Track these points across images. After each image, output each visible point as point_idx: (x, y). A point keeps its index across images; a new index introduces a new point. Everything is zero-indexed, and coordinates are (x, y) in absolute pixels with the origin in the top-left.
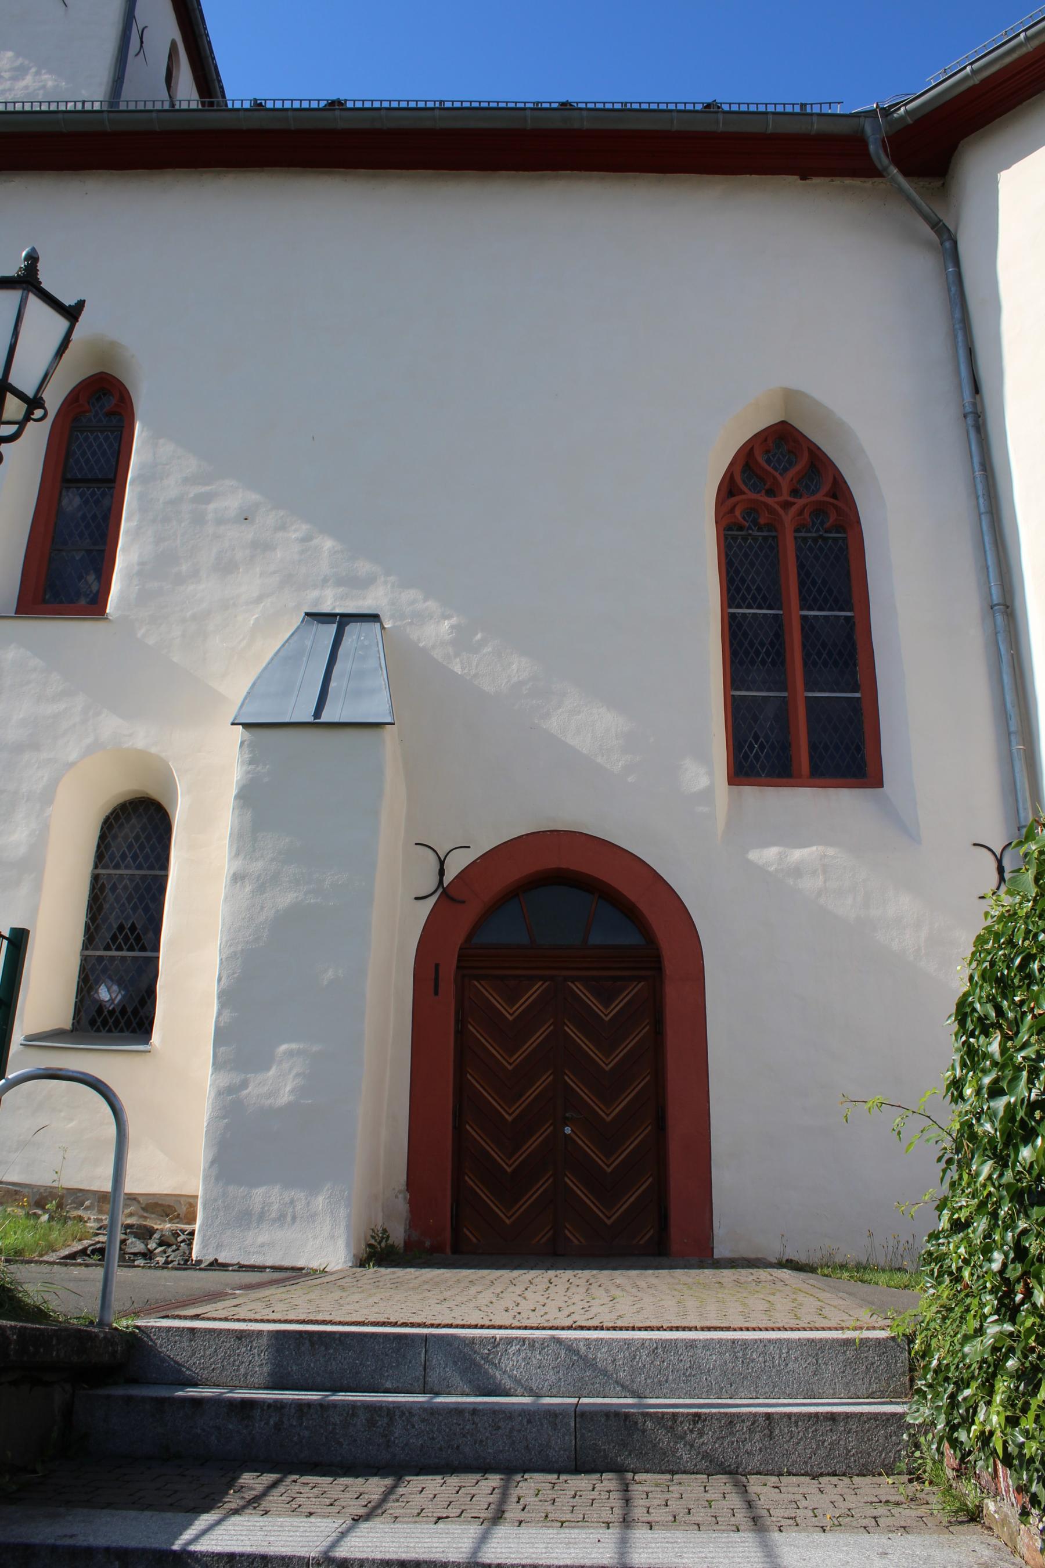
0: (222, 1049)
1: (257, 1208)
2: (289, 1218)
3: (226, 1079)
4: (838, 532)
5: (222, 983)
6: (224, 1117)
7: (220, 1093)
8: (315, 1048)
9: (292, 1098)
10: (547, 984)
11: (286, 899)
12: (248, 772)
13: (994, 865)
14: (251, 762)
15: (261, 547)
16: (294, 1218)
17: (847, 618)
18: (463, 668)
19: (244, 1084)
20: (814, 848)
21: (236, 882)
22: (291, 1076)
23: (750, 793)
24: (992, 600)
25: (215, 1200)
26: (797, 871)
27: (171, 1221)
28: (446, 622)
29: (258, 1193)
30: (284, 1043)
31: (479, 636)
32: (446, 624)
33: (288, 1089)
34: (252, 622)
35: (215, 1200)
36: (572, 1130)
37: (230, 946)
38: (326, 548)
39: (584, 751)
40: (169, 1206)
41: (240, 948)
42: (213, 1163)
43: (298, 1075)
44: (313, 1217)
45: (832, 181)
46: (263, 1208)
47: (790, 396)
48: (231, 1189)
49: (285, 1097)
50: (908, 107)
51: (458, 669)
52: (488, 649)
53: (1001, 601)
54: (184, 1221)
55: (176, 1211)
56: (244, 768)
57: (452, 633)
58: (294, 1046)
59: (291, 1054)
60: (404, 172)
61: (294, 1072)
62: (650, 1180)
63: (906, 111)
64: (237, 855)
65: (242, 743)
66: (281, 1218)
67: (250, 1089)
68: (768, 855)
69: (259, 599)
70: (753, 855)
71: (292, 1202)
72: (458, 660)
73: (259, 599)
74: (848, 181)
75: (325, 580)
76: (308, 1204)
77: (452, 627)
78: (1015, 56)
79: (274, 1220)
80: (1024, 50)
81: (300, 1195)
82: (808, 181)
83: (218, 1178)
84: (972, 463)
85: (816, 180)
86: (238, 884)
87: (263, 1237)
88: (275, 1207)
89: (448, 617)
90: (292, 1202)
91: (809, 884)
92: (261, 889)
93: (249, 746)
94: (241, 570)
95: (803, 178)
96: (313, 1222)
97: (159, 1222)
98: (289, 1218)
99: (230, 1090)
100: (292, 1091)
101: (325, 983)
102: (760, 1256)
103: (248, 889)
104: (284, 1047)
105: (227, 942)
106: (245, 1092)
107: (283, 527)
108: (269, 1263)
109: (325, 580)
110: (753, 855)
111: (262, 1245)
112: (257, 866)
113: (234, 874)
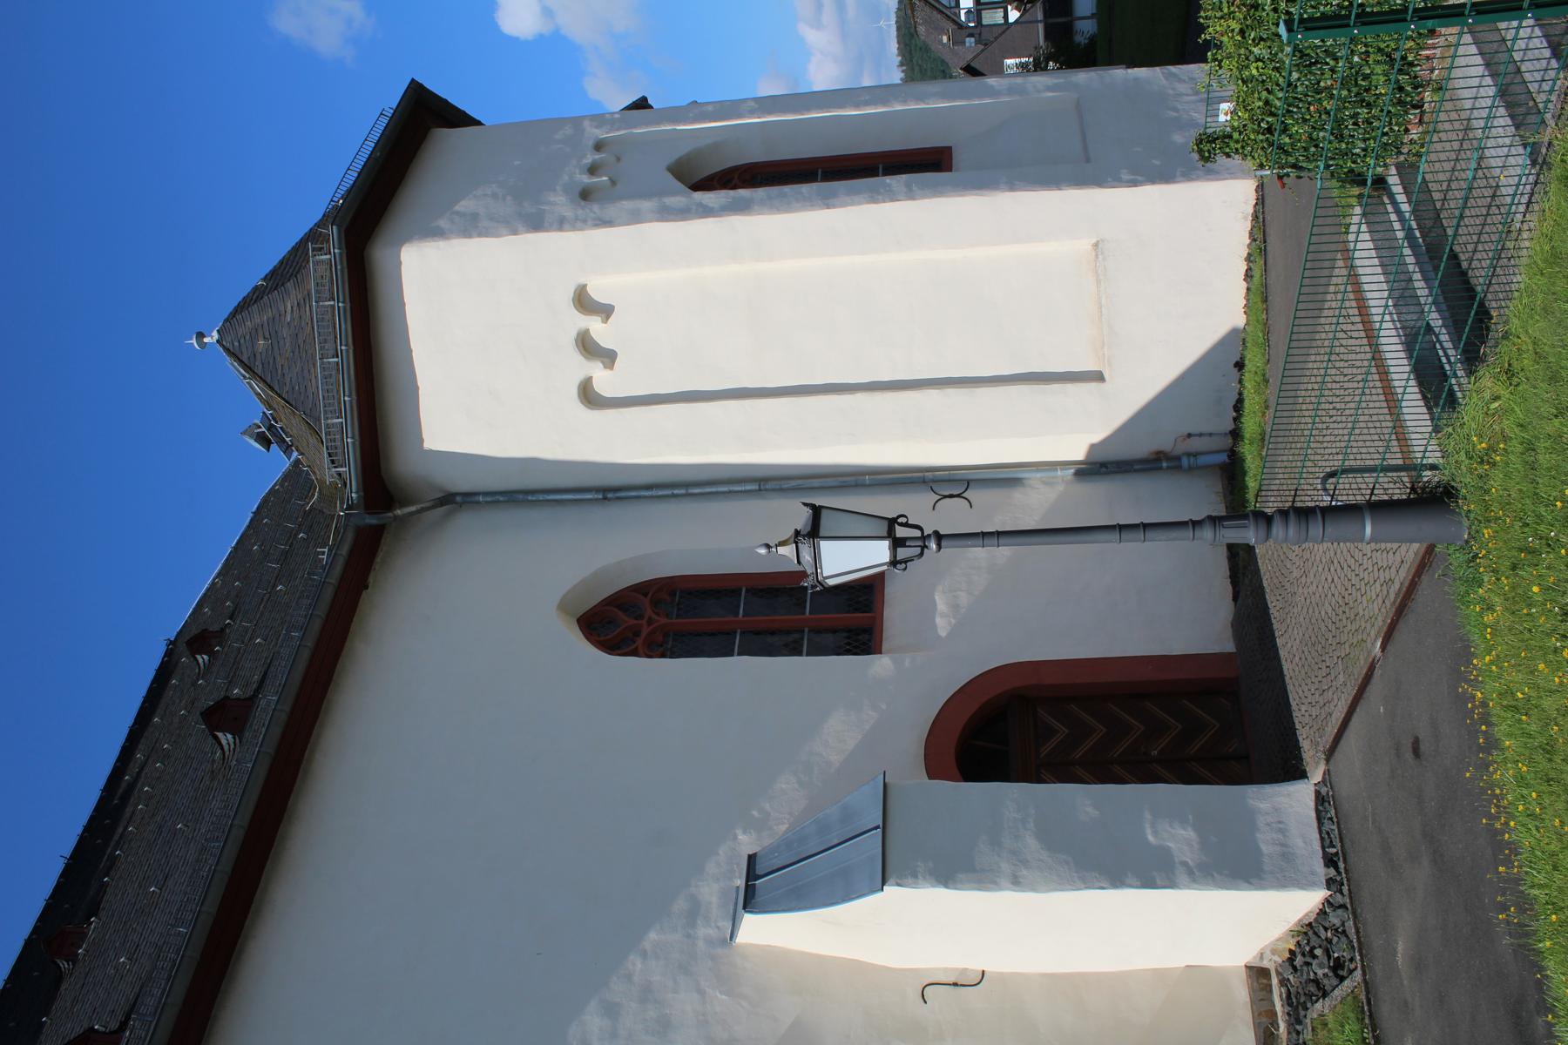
0: (1159, 882)
1: (1278, 848)
2: (1281, 826)
3: (1182, 876)
4: (675, 595)
5: (1105, 886)
6: (1213, 876)
7: (1194, 881)
8: (1148, 816)
9: (1190, 829)
10: (1043, 771)
11: (1032, 843)
12: (924, 878)
13: (947, 500)
14: (915, 876)
15: (647, 994)
16: (1280, 822)
17: (747, 591)
18: (784, 823)
19: (1185, 864)
20: (937, 597)
21: (1020, 882)
22: (1173, 831)
23: (885, 646)
24: (756, 491)
25: (1278, 879)
26: (955, 607)
27: (1277, 1029)
28: (740, 837)
29: (1265, 848)
30: (1147, 839)
31: (755, 813)
32: (741, 837)
33: (1183, 832)
34: (724, 997)
35: (1278, 879)
36: (1155, 750)
37: (1074, 882)
38: (656, 937)
39: (860, 737)
40: (1264, 1033)
41: (1075, 874)
42: (1250, 883)
43: (1171, 826)
44: (1276, 810)
45: (375, 569)
46: (1276, 844)
47: (564, 607)
48: (1266, 868)
49: (1190, 834)
50: (354, 491)
51: (784, 828)
52: (767, 806)
53: (757, 484)
54: (1274, 1018)
55: (1268, 1026)
56: (920, 882)
57: (750, 833)
58: (1149, 831)
59: (1155, 833)
60: (262, 884)
61: (1170, 829)
62: (1184, 701)
63: (357, 492)
64: (995, 883)
65: (899, 885)
66: (1282, 831)
67: (1187, 860)
68: (943, 625)
69: (701, 992)
70: (943, 633)
71: (1268, 824)
72: (775, 828)
73: (701, 992)
74: (378, 559)
75: (688, 936)
76: (1267, 814)
77: (745, 832)
78: (355, 408)
79: (1284, 836)
80: (354, 402)
81: (1261, 821)
82: (370, 585)
83: (1261, 879)
84: (645, 497)
85: (371, 580)
86: (1022, 880)
87: (1299, 842)
88: (1274, 836)
89: (735, 838)
90: (1268, 824)
91: (964, 599)
92: (1025, 863)
93: (900, 879)
94: (668, 1012)
95: (367, 587)
96: (1280, 809)
97: (1280, 1040)
98: (1281, 826)
99: (1190, 872)
100: (1185, 829)
101: (1097, 812)
102: (1230, 625)
103: (1025, 872)
104: (1151, 838)
105: (1070, 885)
106: (1191, 863)
107: (629, 977)
108: (1318, 836)
109: (688, 936)
110: (943, 633)
111: (1305, 843)
112: (1005, 867)
113: (1013, 883)
